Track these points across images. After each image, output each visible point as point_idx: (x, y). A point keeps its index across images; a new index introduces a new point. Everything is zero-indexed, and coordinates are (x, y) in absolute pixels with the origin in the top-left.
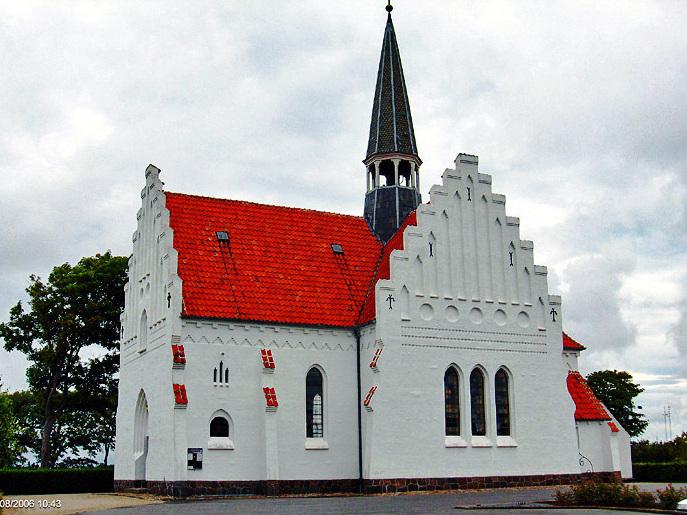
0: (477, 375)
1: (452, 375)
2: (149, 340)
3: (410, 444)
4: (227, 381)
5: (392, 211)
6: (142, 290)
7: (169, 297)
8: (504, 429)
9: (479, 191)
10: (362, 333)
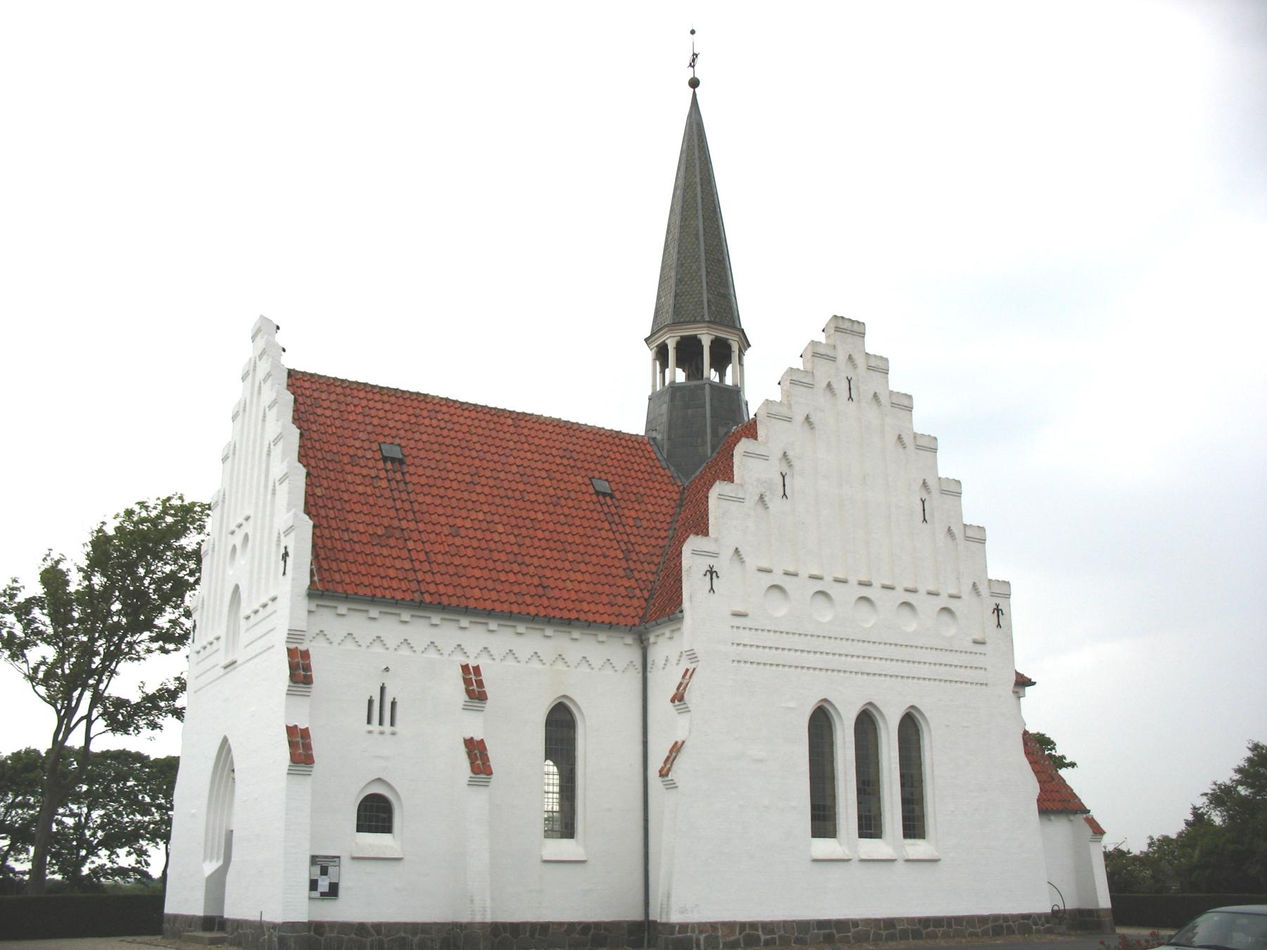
0: (866, 723)
1: (821, 722)
2: (244, 638)
3: (743, 845)
4: (392, 724)
5: (702, 425)
6: (234, 547)
7: (286, 555)
8: (914, 826)
9: (868, 383)
10: (652, 639)
